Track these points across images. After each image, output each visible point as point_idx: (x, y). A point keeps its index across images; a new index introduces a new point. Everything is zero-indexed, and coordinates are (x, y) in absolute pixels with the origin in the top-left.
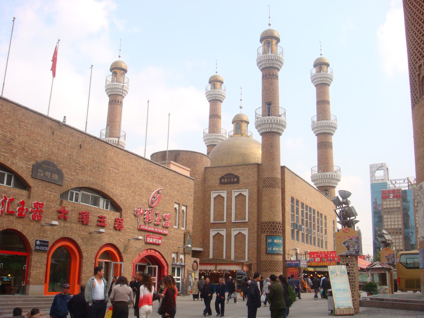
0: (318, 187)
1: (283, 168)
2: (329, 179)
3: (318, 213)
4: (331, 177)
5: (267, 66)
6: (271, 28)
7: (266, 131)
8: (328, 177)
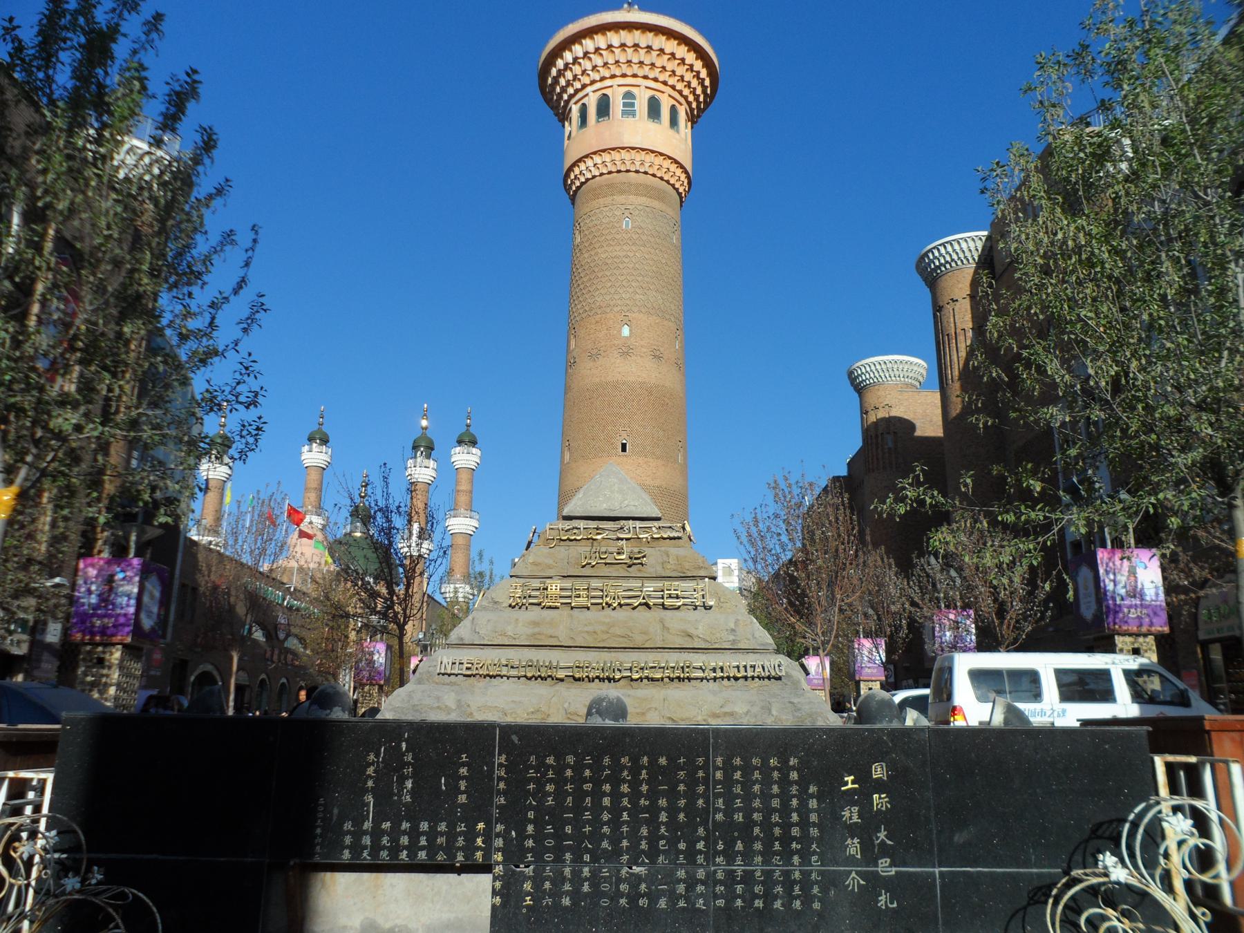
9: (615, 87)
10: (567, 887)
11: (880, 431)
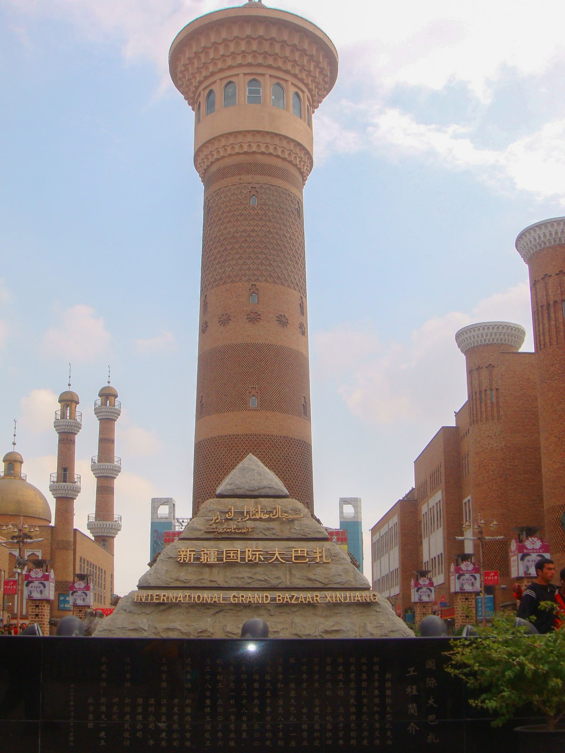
0: (95, 537)
1: (76, 530)
2: (109, 528)
3: (99, 568)
4: (111, 527)
5: (65, 431)
6: (72, 389)
7: (61, 496)
8: (108, 527)
9: (241, 76)
10: (232, 735)
11: (484, 388)
